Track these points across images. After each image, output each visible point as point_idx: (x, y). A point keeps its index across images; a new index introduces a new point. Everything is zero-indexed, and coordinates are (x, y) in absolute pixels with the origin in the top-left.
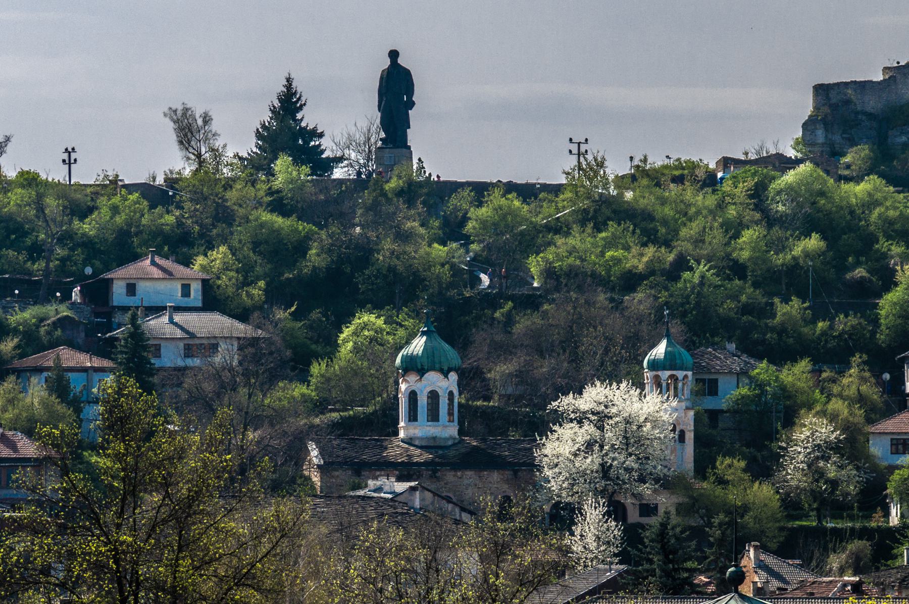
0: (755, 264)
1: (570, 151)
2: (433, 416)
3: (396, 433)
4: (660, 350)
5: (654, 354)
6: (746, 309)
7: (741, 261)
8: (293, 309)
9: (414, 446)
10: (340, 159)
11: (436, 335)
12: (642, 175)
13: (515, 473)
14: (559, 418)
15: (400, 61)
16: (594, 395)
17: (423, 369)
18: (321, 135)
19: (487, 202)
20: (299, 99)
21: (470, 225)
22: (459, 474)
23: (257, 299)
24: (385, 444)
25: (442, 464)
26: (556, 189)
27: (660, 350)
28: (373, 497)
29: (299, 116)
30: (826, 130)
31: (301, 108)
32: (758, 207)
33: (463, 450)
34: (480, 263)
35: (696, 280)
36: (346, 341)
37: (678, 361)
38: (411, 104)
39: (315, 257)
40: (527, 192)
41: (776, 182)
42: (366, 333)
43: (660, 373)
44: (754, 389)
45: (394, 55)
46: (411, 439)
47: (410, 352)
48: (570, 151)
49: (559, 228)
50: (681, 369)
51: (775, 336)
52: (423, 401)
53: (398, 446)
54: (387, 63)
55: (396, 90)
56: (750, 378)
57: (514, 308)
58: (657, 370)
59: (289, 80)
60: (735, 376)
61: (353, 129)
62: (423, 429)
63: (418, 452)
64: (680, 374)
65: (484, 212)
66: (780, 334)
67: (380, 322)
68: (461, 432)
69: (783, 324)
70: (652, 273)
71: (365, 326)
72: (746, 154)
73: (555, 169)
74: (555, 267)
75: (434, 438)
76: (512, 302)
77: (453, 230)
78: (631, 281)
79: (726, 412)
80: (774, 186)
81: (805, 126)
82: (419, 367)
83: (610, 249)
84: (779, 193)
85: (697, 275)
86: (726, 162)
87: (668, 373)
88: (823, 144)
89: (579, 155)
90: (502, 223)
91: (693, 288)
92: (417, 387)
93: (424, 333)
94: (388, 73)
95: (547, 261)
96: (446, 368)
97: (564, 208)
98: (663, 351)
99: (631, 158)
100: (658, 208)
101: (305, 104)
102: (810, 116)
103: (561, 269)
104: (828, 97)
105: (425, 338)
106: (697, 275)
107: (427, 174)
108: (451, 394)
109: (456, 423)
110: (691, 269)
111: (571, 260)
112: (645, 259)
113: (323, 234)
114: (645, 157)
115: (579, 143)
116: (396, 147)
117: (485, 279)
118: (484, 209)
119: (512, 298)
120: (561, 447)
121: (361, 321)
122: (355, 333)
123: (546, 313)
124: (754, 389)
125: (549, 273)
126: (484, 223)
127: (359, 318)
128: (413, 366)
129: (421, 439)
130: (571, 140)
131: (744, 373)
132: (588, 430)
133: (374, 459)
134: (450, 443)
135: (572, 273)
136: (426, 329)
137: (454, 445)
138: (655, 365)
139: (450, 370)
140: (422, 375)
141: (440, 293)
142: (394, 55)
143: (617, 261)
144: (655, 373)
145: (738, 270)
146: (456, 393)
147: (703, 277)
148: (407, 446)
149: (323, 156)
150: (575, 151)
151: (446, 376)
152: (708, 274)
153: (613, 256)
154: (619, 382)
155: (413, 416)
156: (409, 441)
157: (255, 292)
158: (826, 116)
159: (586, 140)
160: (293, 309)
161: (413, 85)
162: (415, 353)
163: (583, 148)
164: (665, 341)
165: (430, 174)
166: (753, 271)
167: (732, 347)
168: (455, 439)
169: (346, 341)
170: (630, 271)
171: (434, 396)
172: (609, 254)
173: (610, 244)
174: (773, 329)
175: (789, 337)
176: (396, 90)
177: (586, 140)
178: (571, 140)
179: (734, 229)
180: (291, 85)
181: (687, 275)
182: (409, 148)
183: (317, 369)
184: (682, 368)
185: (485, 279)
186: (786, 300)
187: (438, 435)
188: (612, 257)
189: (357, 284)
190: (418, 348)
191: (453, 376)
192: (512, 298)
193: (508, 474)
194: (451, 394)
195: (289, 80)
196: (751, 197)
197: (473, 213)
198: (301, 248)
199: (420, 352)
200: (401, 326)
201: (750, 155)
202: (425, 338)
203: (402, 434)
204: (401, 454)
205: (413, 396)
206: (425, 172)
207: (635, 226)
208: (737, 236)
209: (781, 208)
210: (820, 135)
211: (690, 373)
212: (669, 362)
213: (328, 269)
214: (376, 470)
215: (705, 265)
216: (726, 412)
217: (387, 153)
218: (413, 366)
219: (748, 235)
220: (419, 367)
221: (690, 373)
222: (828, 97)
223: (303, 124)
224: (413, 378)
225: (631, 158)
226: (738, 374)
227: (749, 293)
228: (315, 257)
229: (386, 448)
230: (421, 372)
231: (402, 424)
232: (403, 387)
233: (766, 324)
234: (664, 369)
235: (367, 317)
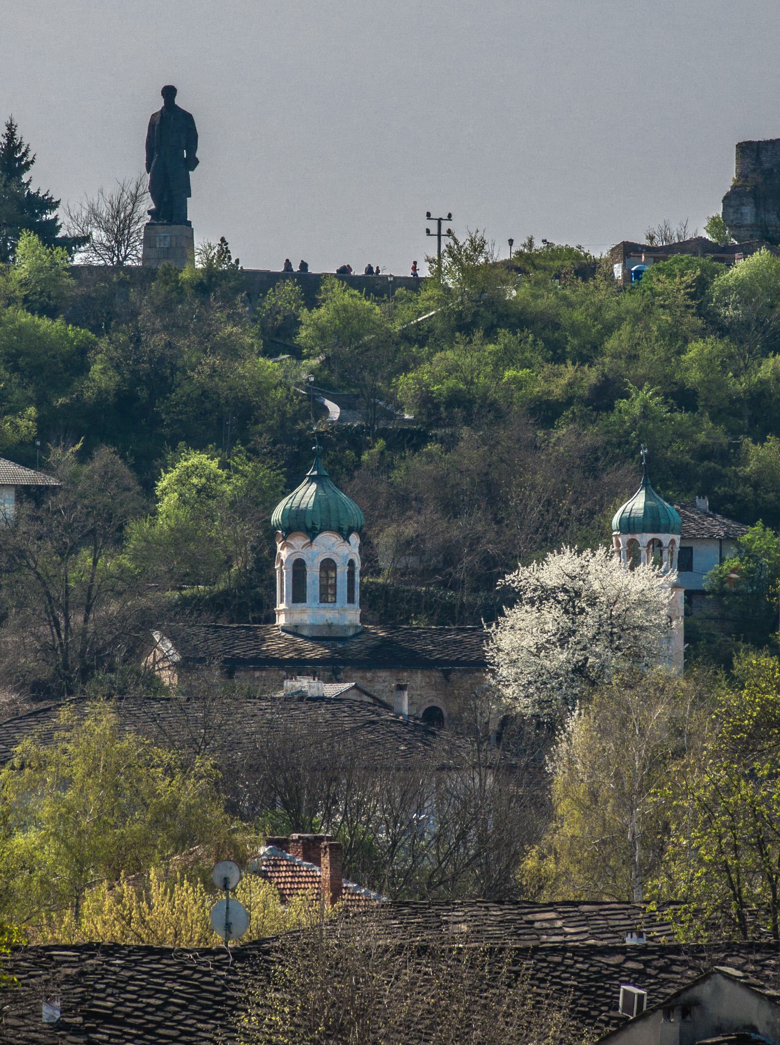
0: (710, 391)
1: (428, 231)
2: (327, 593)
3: (271, 619)
4: (637, 503)
5: (628, 510)
6: (704, 453)
7: (689, 386)
8: (78, 446)
9: (301, 636)
10: (86, 239)
11: (329, 482)
12: (525, 264)
13: (446, 674)
14: (512, 597)
15: (179, 101)
16: (557, 568)
17: (314, 528)
18: (54, 205)
19: (324, 300)
20: (24, 155)
21: (303, 333)
22: (369, 675)
23: (24, 431)
24: (261, 633)
25: (345, 662)
26: (414, 283)
27: (637, 503)
28: (322, 699)
29: (25, 178)
30: (757, 206)
31: (27, 166)
32: (701, 312)
33: (370, 643)
34: (322, 386)
35: (637, 411)
36: (164, 492)
37: (663, 521)
38: (193, 162)
39: (100, 376)
40: (373, 284)
41: (722, 278)
42: (195, 481)
43: (637, 537)
44: (748, 562)
45: (169, 92)
46: (296, 626)
47: (295, 505)
48: (428, 231)
49: (419, 337)
50: (667, 531)
51: (749, 490)
52: (313, 575)
53: (280, 637)
54: (159, 104)
55: (172, 141)
56: (738, 545)
57: (389, 447)
58: (658, 531)
59: (11, 127)
60: (718, 542)
61: (94, 197)
62: (312, 614)
63: (308, 645)
64: (665, 538)
65: (322, 314)
66: (756, 486)
67: (214, 465)
68: (363, 619)
69: (759, 472)
70: (569, 402)
71: (189, 473)
72: (651, 238)
73: (404, 253)
74: (432, 392)
75: (330, 626)
76: (385, 439)
77: (279, 339)
78: (546, 412)
79: (709, 593)
80: (719, 282)
81: (727, 200)
82: (309, 525)
83: (506, 367)
84: (725, 291)
85: (637, 403)
86: (628, 250)
87: (650, 536)
88: (752, 226)
89: (439, 235)
90: (348, 329)
91: (635, 421)
92: (305, 555)
93: (313, 479)
94: (162, 118)
95: (419, 381)
96: (346, 527)
97: (428, 310)
98: (642, 505)
99: (511, 242)
100: (564, 311)
101: (32, 162)
102: (734, 187)
103: (440, 395)
104: (758, 159)
105: (314, 486)
106: (637, 403)
107: (233, 261)
108: (351, 563)
109: (357, 605)
110: (627, 396)
111: (451, 383)
112: (563, 382)
113: (103, 343)
114: (530, 241)
115: (440, 220)
116: (171, 222)
117: (334, 411)
118: (322, 311)
119: (383, 433)
120: (519, 640)
121: (190, 463)
122: (180, 481)
123: (430, 455)
124: (748, 562)
125: (426, 401)
126: (322, 333)
127: (186, 460)
128: (302, 525)
129: (312, 626)
130: (428, 214)
131: (730, 539)
132: (552, 617)
133: (252, 654)
134: (351, 632)
135: (455, 399)
136: (315, 473)
137: (356, 635)
138: (628, 525)
139: (351, 530)
140: (313, 538)
141: (282, 426)
142: (169, 92)
143: (520, 384)
144: (629, 536)
145: (683, 398)
146: (358, 564)
147: (645, 407)
148: (290, 637)
149: (59, 236)
150: (434, 231)
151: (346, 539)
152: (652, 403)
153: (515, 377)
154: (594, 549)
155: (299, 595)
156: (294, 630)
157: (22, 423)
158: (756, 187)
159: (450, 216)
160: (78, 446)
161: (197, 136)
162: (303, 506)
163: (445, 226)
164: (643, 491)
165: (237, 261)
166: (706, 399)
167: (703, 503)
168: (357, 626)
169: (164, 492)
170: (538, 399)
171: (328, 566)
172: (509, 374)
173: (506, 359)
174: (746, 480)
175: (767, 492)
176: (172, 141)
177: (450, 216)
178: (428, 214)
179: (676, 339)
180: (13, 134)
181: (623, 404)
182: (189, 224)
183: (136, 529)
184: (667, 530)
185: (334, 411)
186: (760, 439)
187: (335, 622)
188: (515, 380)
189: (158, 413)
190: (306, 500)
191: (355, 539)
192: (383, 433)
193: (436, 675)
194: (351, 563)
195: (11, 127)
196: (693, 296)
197: (304, 315)
198: (77, 360)
199: (311, 504)
200: (237, 471)
201: (655, 241)
202: (314, 486)
203: (281, 620)
204: (286, 648)
205: (299, 567)
206: (230, 258)
207: (536, 335)
208: (681, 351)
209: (730, 312)
210: (748, 213)
211: (677, 538)
212: (652, 521)
213: (118, 393)
214: (255, 669)
215: (649, 390)
216: (709, 593)
217: (162, 230)
218: (302, 525)
219: (695, 349)
220: (309, 525)
221: (677, 538)
222: (758, 159)
223: (33, 189)
224: (299, 541)
225: (511, 242)
226: (720, 540)
227: (708, 432)
228: (100, 376)
229: (264, 640)
230: (312, 533)
231: (281, 606)
232: (284, 554)
233: (736, 473)
234: (644, 530)
235: (196, 459)
